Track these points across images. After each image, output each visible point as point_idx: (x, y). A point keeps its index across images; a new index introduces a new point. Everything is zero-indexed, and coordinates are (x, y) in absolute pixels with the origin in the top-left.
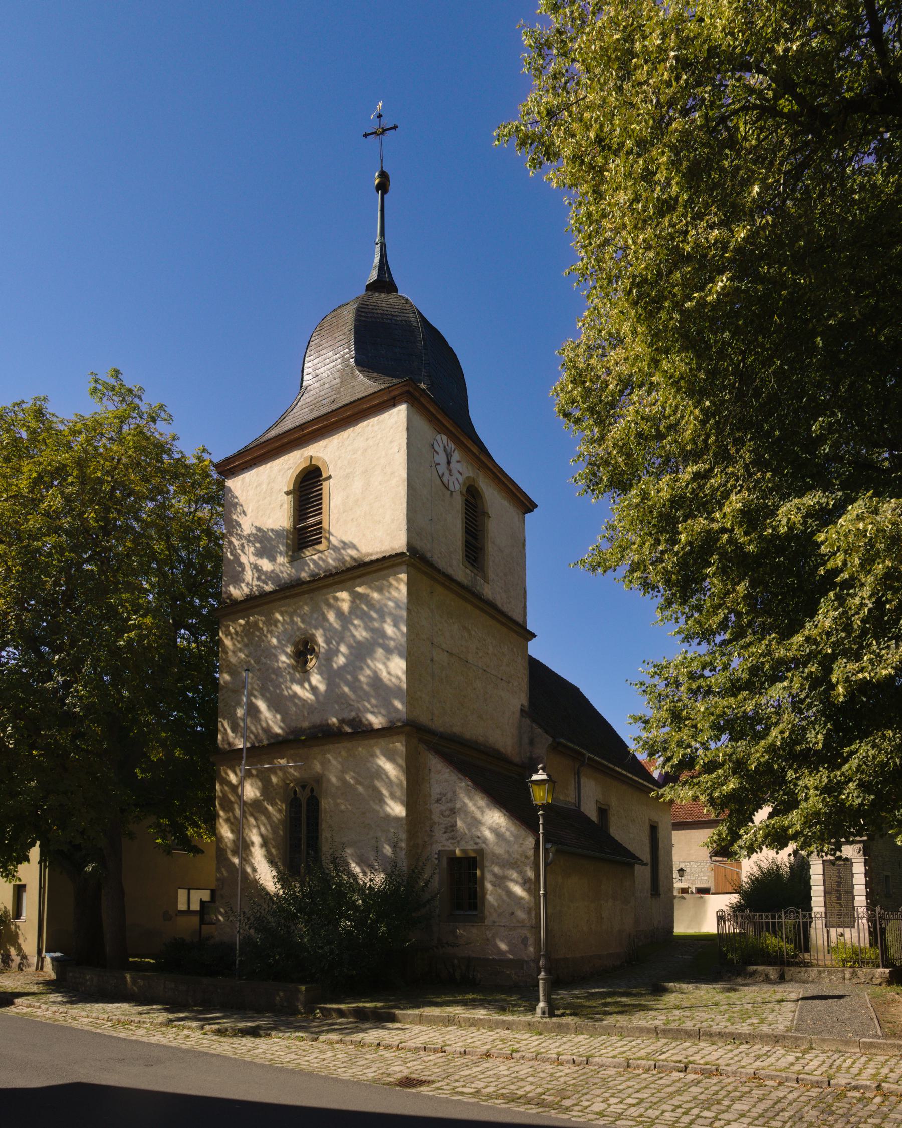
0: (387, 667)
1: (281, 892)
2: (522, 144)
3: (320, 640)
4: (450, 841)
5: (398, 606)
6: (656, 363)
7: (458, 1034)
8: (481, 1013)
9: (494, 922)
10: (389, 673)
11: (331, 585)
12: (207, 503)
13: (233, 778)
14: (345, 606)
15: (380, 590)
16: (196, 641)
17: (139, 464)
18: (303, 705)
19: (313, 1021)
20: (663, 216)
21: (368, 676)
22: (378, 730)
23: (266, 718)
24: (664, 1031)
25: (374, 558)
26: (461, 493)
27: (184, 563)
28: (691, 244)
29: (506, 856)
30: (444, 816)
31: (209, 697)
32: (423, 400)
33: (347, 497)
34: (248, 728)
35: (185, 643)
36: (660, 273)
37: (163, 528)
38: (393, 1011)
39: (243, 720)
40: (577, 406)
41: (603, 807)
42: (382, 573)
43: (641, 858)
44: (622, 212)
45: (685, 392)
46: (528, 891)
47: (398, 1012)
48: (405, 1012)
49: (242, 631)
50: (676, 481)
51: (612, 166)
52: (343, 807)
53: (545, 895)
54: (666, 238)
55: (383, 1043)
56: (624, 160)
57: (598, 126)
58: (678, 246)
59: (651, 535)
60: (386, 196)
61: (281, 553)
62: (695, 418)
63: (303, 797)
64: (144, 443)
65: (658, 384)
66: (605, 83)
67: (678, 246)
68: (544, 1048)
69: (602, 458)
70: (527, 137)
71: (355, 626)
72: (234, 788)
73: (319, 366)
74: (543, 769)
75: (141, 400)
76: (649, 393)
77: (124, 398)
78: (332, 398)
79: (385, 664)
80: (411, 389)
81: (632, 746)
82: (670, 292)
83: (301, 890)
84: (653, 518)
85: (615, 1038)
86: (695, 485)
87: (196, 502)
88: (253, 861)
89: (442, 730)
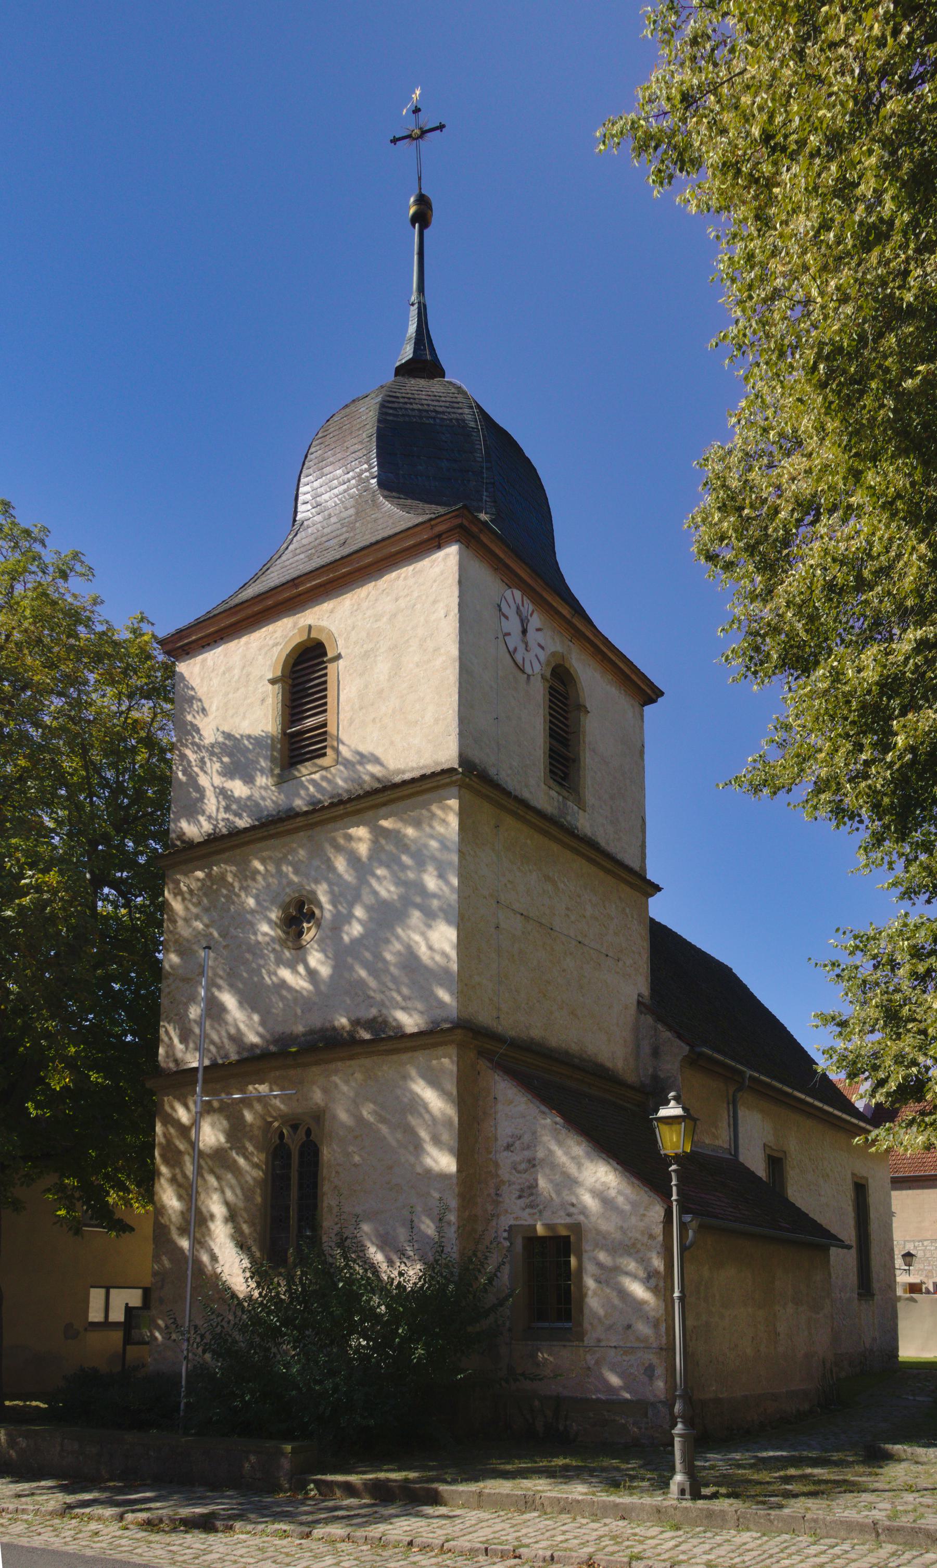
0: (426, 939)
1: (256, 1294)
2: (642, 148)
3: (324, 899)
4: (528, 1210)
5: (444, 846)
6: (856, 475)
7: (541, 1525)
8: (578, 1491)
9: (599, 1340)
10: (430, 948)
11: (341, 817)
12: (148, 698)
13: (183, 1115)
14: (363, 849)
15: (417, 824)
16: (127, 905)
17: (39, 641)
18: (295, 1000)
19: (303, 1503)
20: (869, 251)
21: (399, 953)
22: (413, 1035)
23: (235, 1020)
24: (889, 1529)
25: (407, 776)
26: (543, 677)
27: (110, 787)
28: (913, 291)
29: (618, 1236)
30: (519, 1172)
31: (146, 989)
32: (484, 539)
33: (366, 686)
34: (207, 1036)
35: (110, 908)
36: (862, 338)
37: (77, 735)
38: (435, 1485)
39: (200, 1024)
40: (727, 545)
41: (775, 1154)
42: (420, 798)
43: (839, 1237)
44: (801, 246)
45: (904, 519)
46: (655, 1290)
47: (442, 1487)
48: (453, 1488)
49: (200, 889)
50: (887, 654)
51: (786, 177)
52: (357, 1159)
53: (681, 1299)
54: (872, 284)
55: (418, 1541)
56: (805, 166)
57: (765, 117)
58: (892, 294)
59: (847, 736)
60: (426, 232)
61: (262, 771)
62: (921, 558)
63: (294, 1143)
64: (48, 610)
65: (860, 506)
66: (777, 48)
67: (892, 294)
68: (684, 1552)
69: (769, 624)
70: (649, 136)
71: (378, 878)
72: (184, 1130)
73: (322, 490)
74: (677, 1099)
75: (44, 546)
76: (845, 520)
77: (17, 543)
78: (343, 538)
79: (423, 934)
80: (466, 523)
81: (822, 1063)
82: (880, 366)
83: (289, 1290)
84: (850, 711)
85: (804, 1539)
86: (919, 659)
87: (130, 696)
88: (212, 1244)
89: (512, 1033)
